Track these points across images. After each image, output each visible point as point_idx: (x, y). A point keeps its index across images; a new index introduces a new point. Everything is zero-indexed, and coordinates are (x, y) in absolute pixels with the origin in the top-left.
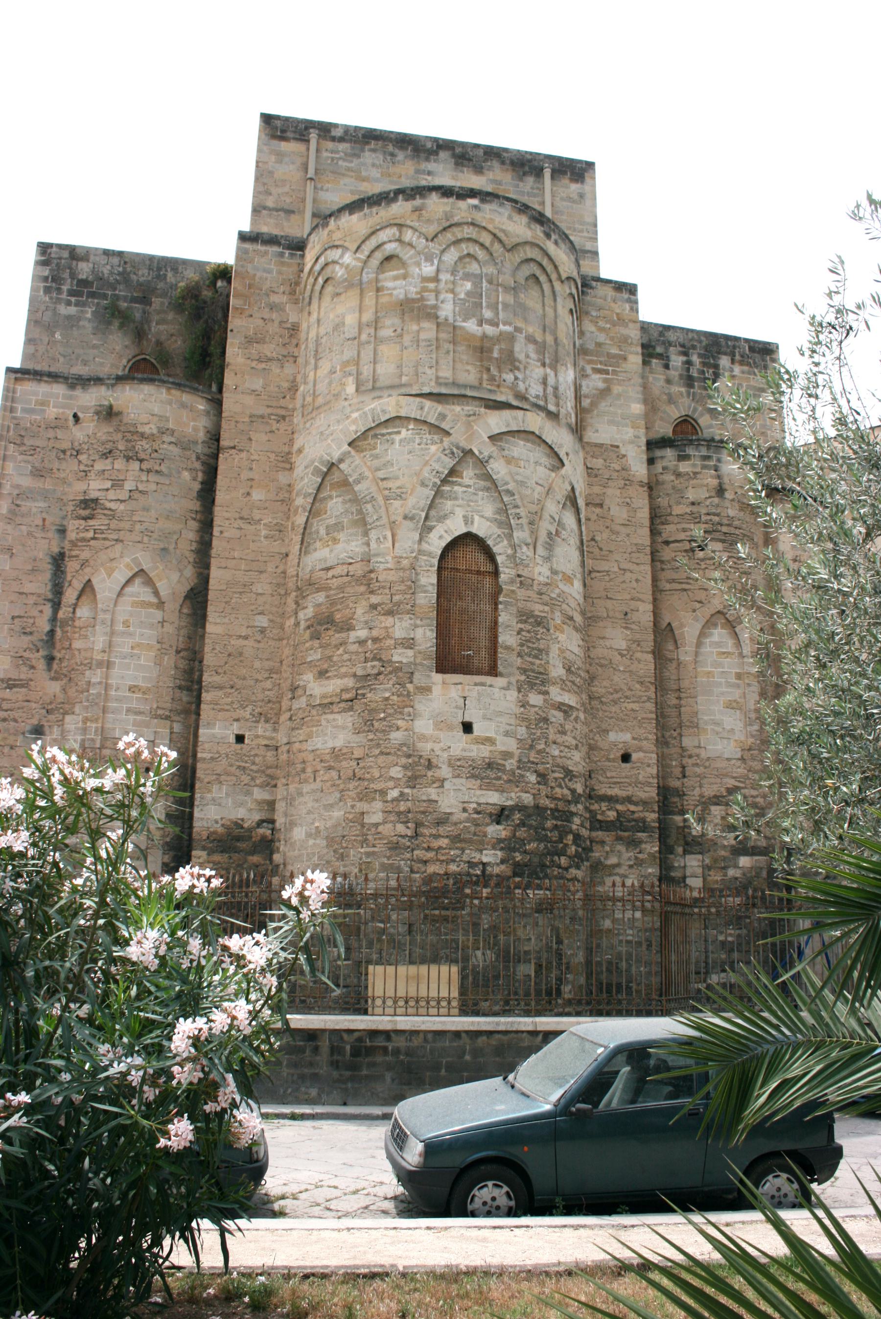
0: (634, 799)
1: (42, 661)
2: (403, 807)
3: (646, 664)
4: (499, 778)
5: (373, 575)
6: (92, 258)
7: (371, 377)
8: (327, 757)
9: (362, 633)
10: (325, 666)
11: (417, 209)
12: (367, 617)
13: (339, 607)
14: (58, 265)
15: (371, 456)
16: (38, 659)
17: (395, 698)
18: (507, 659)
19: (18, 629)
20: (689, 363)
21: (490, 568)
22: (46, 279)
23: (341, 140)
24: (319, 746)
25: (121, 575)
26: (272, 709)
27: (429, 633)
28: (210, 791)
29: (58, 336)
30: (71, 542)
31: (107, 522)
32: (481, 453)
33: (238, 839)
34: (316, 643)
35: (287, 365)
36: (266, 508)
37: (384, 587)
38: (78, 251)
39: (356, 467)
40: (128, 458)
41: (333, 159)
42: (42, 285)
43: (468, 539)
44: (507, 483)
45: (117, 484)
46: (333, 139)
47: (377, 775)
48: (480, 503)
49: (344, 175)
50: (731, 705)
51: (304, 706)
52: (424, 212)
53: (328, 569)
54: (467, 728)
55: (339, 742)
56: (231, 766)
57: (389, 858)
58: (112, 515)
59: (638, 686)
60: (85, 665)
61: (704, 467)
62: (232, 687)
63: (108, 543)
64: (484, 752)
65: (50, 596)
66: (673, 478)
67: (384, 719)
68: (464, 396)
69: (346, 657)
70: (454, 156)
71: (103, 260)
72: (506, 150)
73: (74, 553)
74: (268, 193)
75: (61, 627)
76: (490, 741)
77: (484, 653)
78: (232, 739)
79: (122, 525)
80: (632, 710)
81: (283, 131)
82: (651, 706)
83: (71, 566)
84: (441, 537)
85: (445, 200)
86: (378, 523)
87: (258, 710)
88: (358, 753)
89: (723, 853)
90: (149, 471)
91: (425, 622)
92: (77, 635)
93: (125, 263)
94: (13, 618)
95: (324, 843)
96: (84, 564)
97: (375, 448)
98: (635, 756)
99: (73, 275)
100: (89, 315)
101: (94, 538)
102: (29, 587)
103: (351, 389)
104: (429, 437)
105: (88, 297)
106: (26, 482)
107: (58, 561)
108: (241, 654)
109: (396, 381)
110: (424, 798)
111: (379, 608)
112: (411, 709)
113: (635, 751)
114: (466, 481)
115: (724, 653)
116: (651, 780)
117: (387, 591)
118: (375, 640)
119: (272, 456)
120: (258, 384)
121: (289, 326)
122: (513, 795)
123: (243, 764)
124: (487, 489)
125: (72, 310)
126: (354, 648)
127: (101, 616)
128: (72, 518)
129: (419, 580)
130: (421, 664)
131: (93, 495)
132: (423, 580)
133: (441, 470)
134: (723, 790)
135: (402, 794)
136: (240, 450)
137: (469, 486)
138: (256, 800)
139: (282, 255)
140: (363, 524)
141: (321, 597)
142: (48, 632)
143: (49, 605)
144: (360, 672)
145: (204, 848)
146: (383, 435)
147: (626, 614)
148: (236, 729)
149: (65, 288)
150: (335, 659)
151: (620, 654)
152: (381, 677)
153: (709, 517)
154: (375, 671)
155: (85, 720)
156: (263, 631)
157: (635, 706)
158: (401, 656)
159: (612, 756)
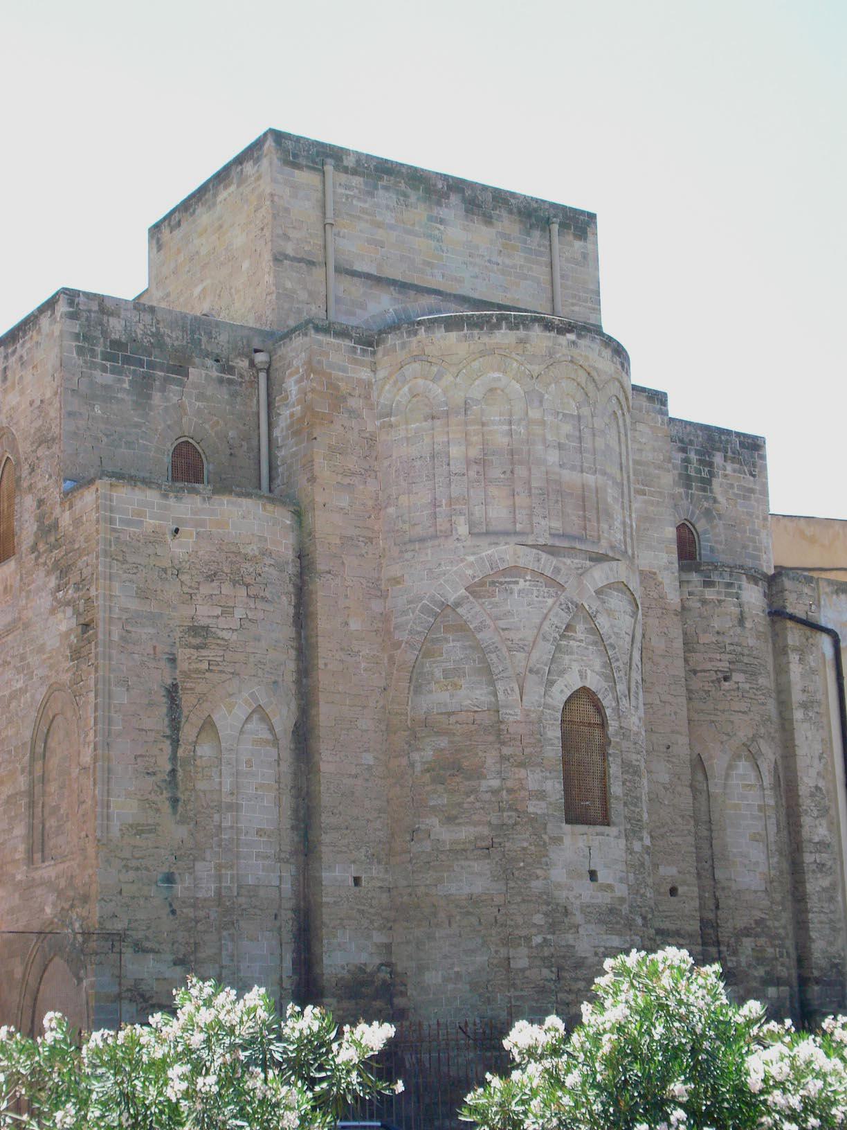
0: (682, 932)
1: (167, 803)
2: (546, 952)
3: (685, 799)
4: (618, 923)
5: (502, 727)
6: (123, 313)
7: (483, 520)
9: (495, 783)
10: (454, 812)
11: (521, 341)
13: (467, 754)
14: (88, 319)
16: (163, 800)
17: (533, 848)
18: (617, 809)
20: (687, 461)
21: (597, 720)
22: (77, 337)
23: (355, 172)
24: (453, 891)
25: (241, 711)
26: (383, 849)
27: (557, 786)
28: (335, 936)
30: (182, 672)
31: (221, 653)
32: (590, 607)
33: (363, 984)
34: (440, 788)
35: (369, 480)
36: (363, 639)
38: (108, 304)
39: (477, 613)
40: (235, 583)
41: (347, 196)
42: (74, 344)
43: (584, 693)
44: (610, 638)
46: (346, 170)
47: (520, 920)
48: (591, 657)
49: (359, 218)
50: (755, 838)
51: (429, 849)
52: (528, 345)
53: (450, 714)
54: (593, 875)
55: (479, 886)
57: (537, 1001)
58: (226, 646)
59: (680, 820)
61: (727, 595)
62: (347, 828)
63: (224, 676)
64: (604, 899)
65: (168, 732)
66: (699, 605)
67: (524, 868)
69: (478, 805)
70: (464, 200)
71: (133, 316)
72: (513, 195)
73: (189, 685)
74: (286, 237)
76: (609, 887)
77: (598, 804)
78: (351, 882)
80: (677, 844)
81: (295, 156)
82: (691, 839)
83: (186, 700)
84: (562, 691)
85: (548, 334)
86: (505, 675)
88: (499, 900)
89: (755, 984)
90: (256, 597)
91: (555, 774)
93: (158, 322)
95: (468, 987)
96: (202, 698)
97: (494, 596)
98: (681, 890)
99: (105, 333)
100: (126, 386)
101: (209, 670)
103: (463, 529)
104: (546, 590)
105: (123, 364)
106: (133, 605)
107: (172, 693)
108: (353, 793)
109: (509, 527)
110: (563, 943)
111: (511, 760)
112: (547, 859)
113: (681, 885)
114: (580, 636)
115: (748, 785)
116: (694, 913)
117: (519, 743)
118: (510, 791)
119: (364, 581)
121: (367, 435)
122: (628, 938)
123: (363, 908)
124: (595, 643)
125: (108, 378)
126: (487, 796)
127: (226, 756)
128: (181, 646)
129: (545, 734)
130: (553, 815)
131: (203, 622)
132: (550, 734)
133: (559, 625)
134: (752, 922)
135: (545, 939)
136: (335, 575)
137: (581, 641)
138: (376, 944)
139: (354, 350)
140: (488, 673)
141: (443, 742)
142: (170, 772)
143: (168, 742)
144: (495, 821)
145: (334, 996)
146: (501, 583)
147: (668, 747)
148: (353, 871)
149: (99, 349)
150: (465, 806)
151: (664, 788)
152: (518, 827)
153: (732, 648)
155: (219, 867)
156: (369, 768)
157: (679, 840)
158: (534, 807)
159: (662, 890)
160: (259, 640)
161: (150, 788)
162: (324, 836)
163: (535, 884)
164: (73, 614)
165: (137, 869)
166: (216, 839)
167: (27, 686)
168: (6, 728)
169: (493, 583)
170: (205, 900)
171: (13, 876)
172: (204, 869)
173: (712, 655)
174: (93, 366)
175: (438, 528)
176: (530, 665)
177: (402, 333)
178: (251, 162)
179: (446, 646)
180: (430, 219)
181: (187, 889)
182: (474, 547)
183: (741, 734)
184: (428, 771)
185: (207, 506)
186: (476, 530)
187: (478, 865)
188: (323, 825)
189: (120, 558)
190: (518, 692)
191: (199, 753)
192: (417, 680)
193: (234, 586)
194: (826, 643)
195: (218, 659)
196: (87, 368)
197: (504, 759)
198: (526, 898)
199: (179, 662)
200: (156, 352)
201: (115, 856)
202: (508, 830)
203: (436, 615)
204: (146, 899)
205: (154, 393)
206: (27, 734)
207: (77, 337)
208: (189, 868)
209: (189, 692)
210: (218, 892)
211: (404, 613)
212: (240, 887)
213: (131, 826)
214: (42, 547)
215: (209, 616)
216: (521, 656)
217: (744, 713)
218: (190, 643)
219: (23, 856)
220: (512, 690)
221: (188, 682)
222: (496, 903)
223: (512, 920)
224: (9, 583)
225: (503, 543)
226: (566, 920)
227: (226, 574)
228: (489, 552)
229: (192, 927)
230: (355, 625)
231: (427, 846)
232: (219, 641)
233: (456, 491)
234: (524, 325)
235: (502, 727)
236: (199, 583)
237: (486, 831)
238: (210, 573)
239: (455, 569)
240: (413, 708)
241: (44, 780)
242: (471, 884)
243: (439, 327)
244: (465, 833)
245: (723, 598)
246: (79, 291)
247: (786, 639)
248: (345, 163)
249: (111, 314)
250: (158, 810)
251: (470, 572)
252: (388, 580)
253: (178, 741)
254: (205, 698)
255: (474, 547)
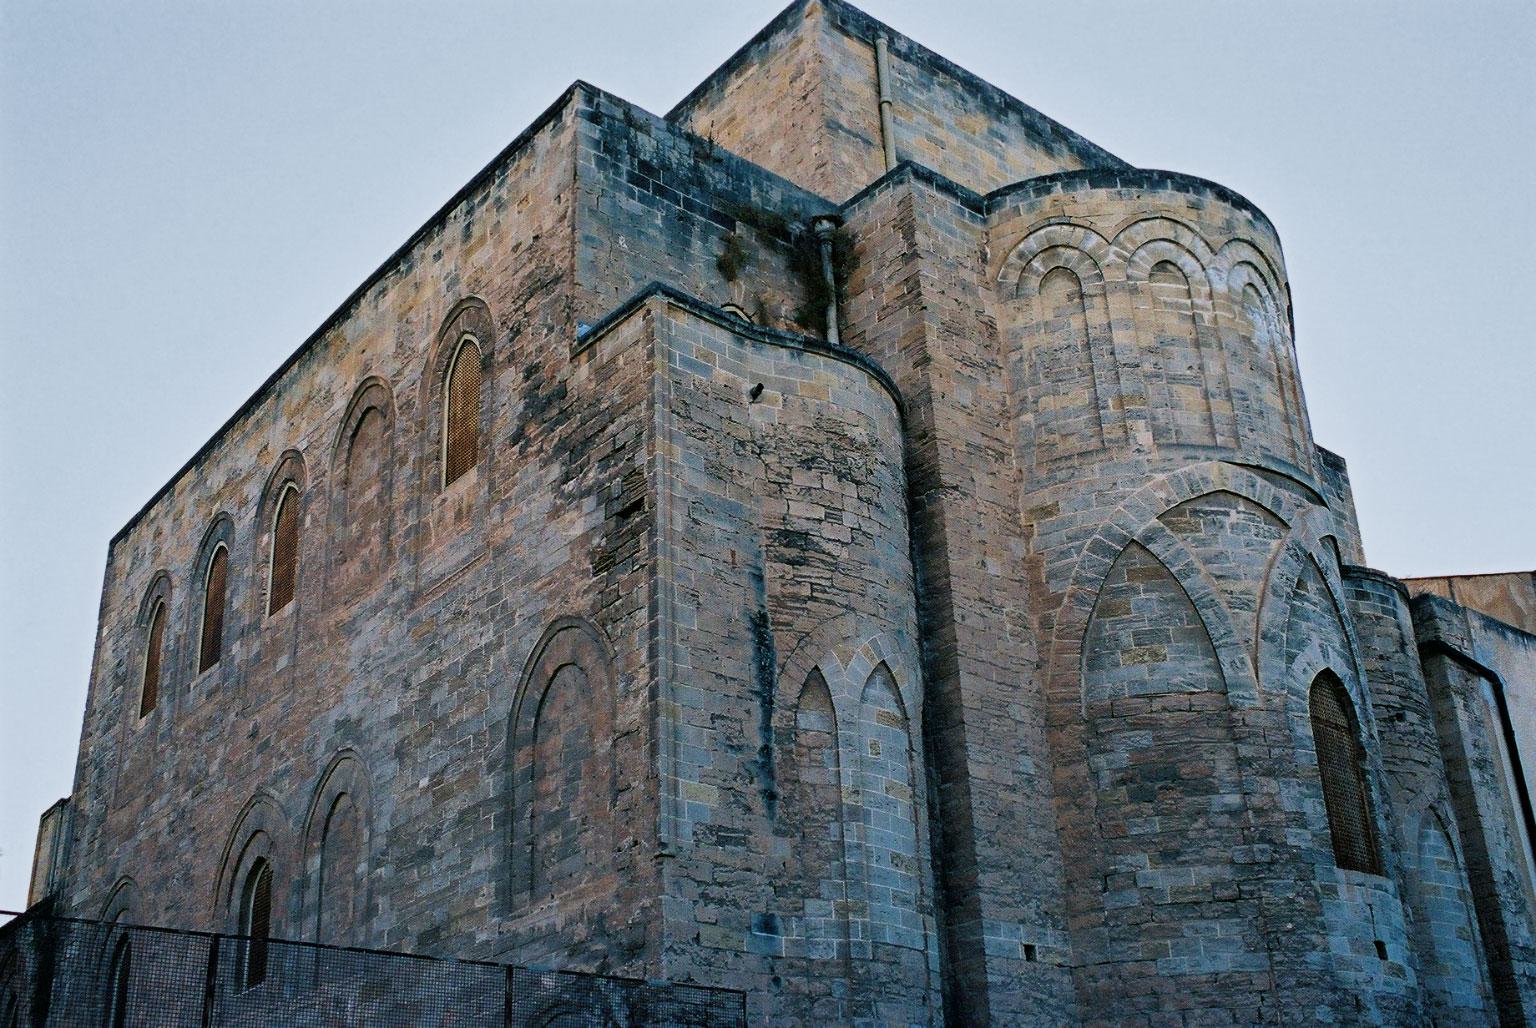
1: (759, 798)
5: (1235, 715)
8: (1206, 988)
9: (1234, 799)
10: (1173, 844)
12: (1234, 777)
15: (1195, 540)
16: (753, 790)
17: (1301, 900)
19: (721, 738)
21: (1342, 721)
23: (906, 58)
24: (1186, 968)
25: (862, 666)
27: (1319, 808)
29: (622, 241)
34: (1147, 808)
37: (1254, 734)
42: (593, 152)
45: (833, 515)
53: (1151, 697)
55: (1226, 961)
56: (1027, 997)
58: (834, 567)
60: (827, 813)
65: (757, 688)
68: (1290, 478)
73: (783, 618)
75: (778, 742)
78: (1022, 955)
79: (850, 583)
81: (844, 22)
83: (781, 640)
85: (1224, 204)
87: (1044, 907)
88: (1261, 982)
90: (869, 501)
92: (805, 759)
94: (714, 718)
96: (804, 637)
99: (633, 151)
100: (659, 222)
102: (728, 668)
103: (1143, 436)
104: (1266, 527)
105: (654, 193)
107: (759, 624)
109: (1207, 441)
111: (1255, 765)
115: (1444, 862)
118: (1259, 812)
120: (966, 397)
121: (986, 319)
125: (635, 206)
126: (1224, 820)
128: (770, 560)
130: (1321, 853)
133: (1290, 576)
140: (1205, 639)
141: (1144, 738)
142: (762, 749)
143: (758, 702)
144: (1241, 859)
146: (1206, 513)
150: (1192, 834)
152: (1277, 867)
154: (1266, 858)
155: (844, 910)
158: (1296, 838)
160: (877, 565)
161: (736, 771)
162: (981, 876)
163: (1314, 957)
164: (599, 504)
165: (721, 902)
166: (835, 863)
167: (501, 637)
168: (457, 710)
169: (1195, 512)
170: (825, 964)
171: (471, 937)
172: (820, 912)
173: (1381, 686)
174: (617, 186)
175: (1106, 436)
176: (1263, 627)
177: (1027, 192)
178: (784, 31)
179: (1133, 600)
180: (991, 132)
181: (796, 943)
182: (1164, 460)
183: (1427, 791)
184: (1123, 782)
185: (796, 363)
186: (1162, 441)
187: (1222, 927)
188: (979, 859)
189: (682, 412)
190: (1250, 665)
191: (802, 724)
192: (1095, 651)
193: (839, 480)
194: (1485, 687)
195: (823, 582)
196: (608, 185)
197: (1241, 763)
198: (1302, 979)
199: (767, 583)
200: (695, 190)
201: (688, 876)
202: (1262, 872)
203: (1117, 555)
204: (736, 955)
205: (693, 240)
206: (502, 710)
207: (596, 144)
208: (796, 909)
209: (784, 628)
210: (845, 950)
211: (1064, 554)
212: (876, 945)
213: (710, 828)
214: (532, 430)
215: (808, 519)
216: (1246, 615)
217: (1424, 764)
218: (782, 555)
219: (492, 900)
220: (1243, 663)
221: (781, 613)
222: (1256, 988)
223: (1286, 1014)
224: (464, 505)
225: (1203, 458)
226: (1361, 1018)
227: (829, 461)
228: (1186, 469)
229: (806, 1009)
230: (994, 568)
231: (1134, 898)
232: (824, 557)
233: (1126, 385)
234: (1194, 188)
235: (1235, 715)
236: (790, 468)
237: (1227, 874)
238: (805, 457)
239: (1139, 490)
240: (1088, 691)
241: (534, 774)
242: (1214, 957)
243: (1082, 183)
244: (1196, 876)
245: (1380, 614)
246: (599, 90)
247: (1445, 677)
248: (897, 46)
249: (640, 128)
250: (748, 809)
251: (1162, 495)
252: (1032, 511)
253: (772, 702)
254: (807, 639)
255: (1164, 460)
